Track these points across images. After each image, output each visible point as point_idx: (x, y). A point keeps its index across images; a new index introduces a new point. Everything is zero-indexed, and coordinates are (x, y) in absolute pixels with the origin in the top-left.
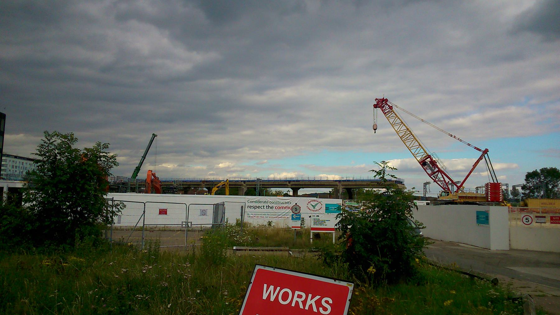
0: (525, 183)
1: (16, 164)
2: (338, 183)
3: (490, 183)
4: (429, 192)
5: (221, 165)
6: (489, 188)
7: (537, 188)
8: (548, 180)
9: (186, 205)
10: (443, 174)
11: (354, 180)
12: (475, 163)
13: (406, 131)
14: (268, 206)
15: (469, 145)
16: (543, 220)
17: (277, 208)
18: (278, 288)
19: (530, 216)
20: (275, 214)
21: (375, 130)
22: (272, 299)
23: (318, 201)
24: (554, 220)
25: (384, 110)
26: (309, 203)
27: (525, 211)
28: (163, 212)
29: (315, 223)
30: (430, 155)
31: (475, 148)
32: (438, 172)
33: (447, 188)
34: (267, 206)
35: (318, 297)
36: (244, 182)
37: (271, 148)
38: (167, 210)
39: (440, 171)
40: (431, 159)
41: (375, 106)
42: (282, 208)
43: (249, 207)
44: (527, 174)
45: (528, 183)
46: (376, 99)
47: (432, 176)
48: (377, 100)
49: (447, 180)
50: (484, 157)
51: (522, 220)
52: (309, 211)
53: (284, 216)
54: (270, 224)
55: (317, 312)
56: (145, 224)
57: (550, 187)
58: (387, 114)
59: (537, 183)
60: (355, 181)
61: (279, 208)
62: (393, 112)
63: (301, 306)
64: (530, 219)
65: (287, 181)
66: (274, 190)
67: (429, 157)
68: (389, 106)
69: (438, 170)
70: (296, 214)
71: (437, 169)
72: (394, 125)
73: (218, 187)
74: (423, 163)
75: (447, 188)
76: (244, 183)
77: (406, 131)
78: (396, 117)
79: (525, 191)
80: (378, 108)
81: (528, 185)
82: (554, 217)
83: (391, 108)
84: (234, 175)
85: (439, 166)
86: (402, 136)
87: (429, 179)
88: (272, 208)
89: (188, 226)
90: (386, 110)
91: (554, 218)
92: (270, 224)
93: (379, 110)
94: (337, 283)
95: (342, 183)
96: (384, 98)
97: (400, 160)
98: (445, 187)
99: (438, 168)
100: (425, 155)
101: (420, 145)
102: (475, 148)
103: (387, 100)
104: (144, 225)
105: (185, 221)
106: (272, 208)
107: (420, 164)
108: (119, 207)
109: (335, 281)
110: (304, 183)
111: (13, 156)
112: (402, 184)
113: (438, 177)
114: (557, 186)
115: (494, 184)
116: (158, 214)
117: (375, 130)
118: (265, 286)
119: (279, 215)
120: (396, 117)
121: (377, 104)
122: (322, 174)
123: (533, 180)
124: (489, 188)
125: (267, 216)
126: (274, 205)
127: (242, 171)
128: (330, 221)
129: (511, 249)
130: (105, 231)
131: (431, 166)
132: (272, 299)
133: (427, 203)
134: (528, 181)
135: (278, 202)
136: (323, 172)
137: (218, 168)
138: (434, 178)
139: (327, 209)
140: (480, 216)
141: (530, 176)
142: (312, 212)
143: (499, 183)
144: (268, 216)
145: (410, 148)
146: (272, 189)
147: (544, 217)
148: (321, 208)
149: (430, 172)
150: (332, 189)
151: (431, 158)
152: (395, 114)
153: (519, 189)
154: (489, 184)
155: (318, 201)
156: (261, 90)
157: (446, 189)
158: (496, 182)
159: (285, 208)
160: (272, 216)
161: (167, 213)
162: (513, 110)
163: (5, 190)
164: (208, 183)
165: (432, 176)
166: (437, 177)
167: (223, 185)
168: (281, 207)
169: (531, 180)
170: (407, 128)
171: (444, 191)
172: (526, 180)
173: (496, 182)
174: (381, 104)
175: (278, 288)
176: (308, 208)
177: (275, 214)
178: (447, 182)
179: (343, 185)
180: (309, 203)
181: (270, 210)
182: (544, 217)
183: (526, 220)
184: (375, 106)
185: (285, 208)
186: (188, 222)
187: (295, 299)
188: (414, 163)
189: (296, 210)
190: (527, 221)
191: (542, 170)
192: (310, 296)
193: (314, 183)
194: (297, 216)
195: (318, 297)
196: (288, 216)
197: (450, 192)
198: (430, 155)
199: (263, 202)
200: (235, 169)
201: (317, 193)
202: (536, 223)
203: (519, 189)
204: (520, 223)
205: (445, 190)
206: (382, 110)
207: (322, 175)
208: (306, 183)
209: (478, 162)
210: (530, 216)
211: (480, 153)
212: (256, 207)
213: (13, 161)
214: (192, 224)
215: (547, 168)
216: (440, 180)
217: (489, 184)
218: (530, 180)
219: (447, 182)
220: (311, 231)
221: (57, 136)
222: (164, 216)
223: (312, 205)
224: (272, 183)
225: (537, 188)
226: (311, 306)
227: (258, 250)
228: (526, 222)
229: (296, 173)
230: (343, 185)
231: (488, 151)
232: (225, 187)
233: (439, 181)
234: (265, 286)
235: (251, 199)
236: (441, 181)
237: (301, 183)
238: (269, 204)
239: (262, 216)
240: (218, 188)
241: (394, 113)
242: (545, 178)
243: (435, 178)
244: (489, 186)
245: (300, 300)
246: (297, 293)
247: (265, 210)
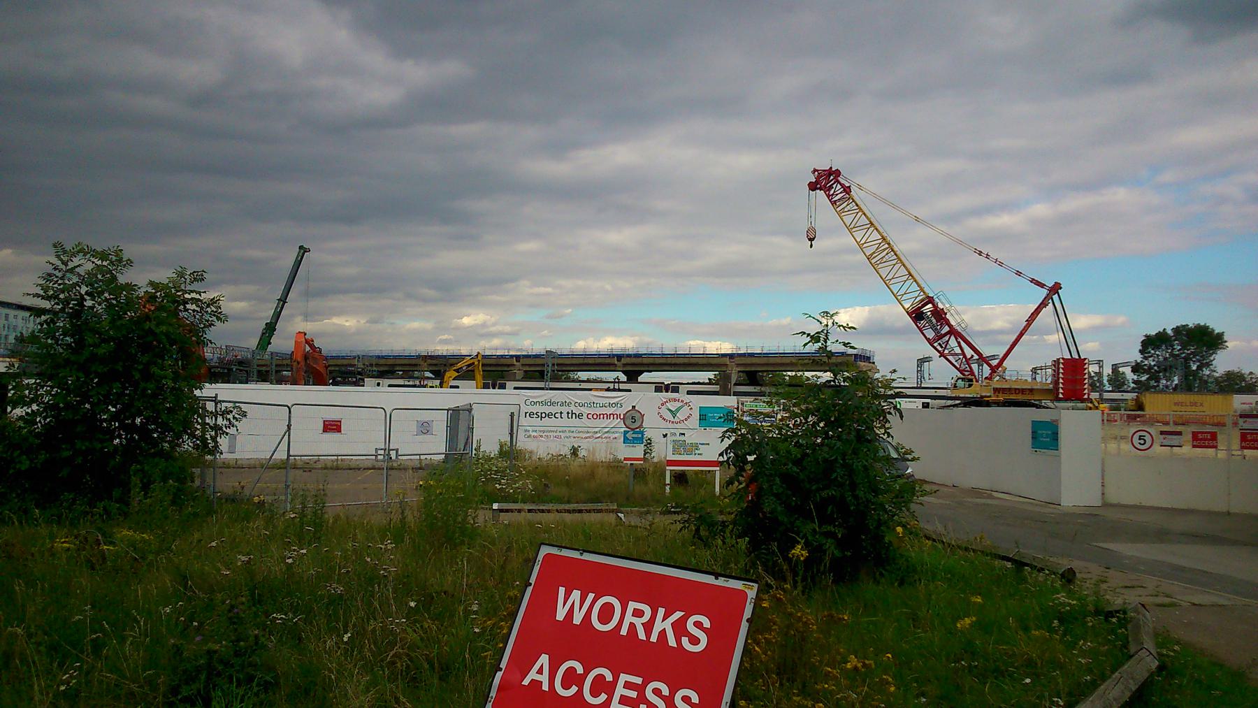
0: (1139, 358)
2: (727, 360)
3: (1063, 359)
4: (929, 379)
5: (466, 321)
6: (1061, 371)
7: (1166, 369)
8: (1189, 352)
9: (385, 411)
10: (960, 340)
11: (764, 354)
12: (1032, 314)
13: (880, 244)
14: (570, 412)
15: (1019, 273)
16: (1175, 440)
17: (590, 416)
18: (591, 596)
20: (586, 429)
21: (811, 240)
22: (578, 619)
23: (682, 401)
24: (1248, 441)
25: (833, 195)
26: (662, 404)
28: (332, 427)
29: (675, 452)
30: (933, 297)
31: (1033, 281)
32: (949, 335)
33: (968, 371)
34: (568, 413)
35: (678, 615)
36: (518, 358)
37: (580, 282)
38: (340, 421)
39: (953, 332)
40: (935, 306)
41: (813, 187)
42: (602, 416)
43: (528, 414)
44: (1144, 338)
45: (1146, 358)
46: (815, 170)
47: (936, 345)
48: (816, 173)
49: (969, 352)
50: (1050, 301)
53: (606, 435)
54: (575, 452)
55: (676, 646)
56: (291, 453)
57: (1194, 368)
58: (838, 204)
59: (1165, 359)
60: (766, 355)
61: (595, 417)
62: (852, 199)
63: (642, 635)
64: (1148, 438)
65: (614, 356)
66: (583, 375)
67: (930, 300)
68: (842, 185)
69: (948, 329)
70: (633, 429)
71: (946, 329)
72: (854, 230)
73: (457, 371)
74: (917, 315)
75: (968, 371)
76: (516, 361)
77: (880, 244)
78: (858, 211)
79: (1138, 376)
80: (818, 191)
81: (1146, 362)
82: (1200, 432)
83: (847, 190)
84: (496, 342)
85: (953, 323)
86: (871, 255)
87: (929, 351)
88: (580, 416)
89: (391, 458)
90: (837, 195)
91: (1199, 435)
92: (575, 452)
93: (820, 193)
94: (721, 582)
95: (737, 360)
96: (831, 168)
97: (867, 308)
98: (963, 367)
99: (949, 326)
100: (921, 297)
101: (910, 274)
102: (1033, 281)
103: (838, 173)
104: (289, 455)
105: (383, 447)
106: (580, 416)
107: (911, 317)
108: (230, 416)
109: (717, 578)
110: (651, 361)
112: (870, 363)
113: (948, 347)
114: (1208, 365)
115: (1072, 359)
116: (321, 431)
117: (811, 240)
118: (562, 590)
119: (597, 432)
120: (858, 211)
121: (817, 182)
122: (692, 340)
123: (1157, 353)
124: (1061, 371)
125: (568, 434)
126: (585, 411)
127: (515, 334)
128: (708, 444)
129: (1106, 505)
131: (934, 321)
132: (578, 619)
133: (923, 403)
134: (1146, 355)
135: (594, 403)
136: (697, 336)
137: (458, 328)
138: (940, 349)
139: (703, 418)
141: (1150, 343)
142: (671, 426)
143: (1082, 358)
144: (571, 434)
145: (887, 282)
146: (579, 373)
148: (689, 417)
149: (931, 334)
150: (714, 373)
151: (933, 305)
152: (857, 205)
153: (1127, 371)
154: (1061, 361)
155: (682, 401)
156: (558, 149)
157: (967, 373)
158: (1077, 357)
159: (608, 416)
160: (581, 435)
161: (342, 429)
162: (1120, 195)
164: (434, 362)
165: (936, 345)
166: (946, 346)
167: (469, 366)
168: (600, 415)
169: (1153, 352)
170: (882, 237)
171: (962, 376)
172: (1141, 352)
173: (1077, 357)
174: (825, 180)
175: (591, 596)
176: (661, 416)
177: (586, 429)
178: (969, 357)
179: (738, 365)
180: (662, 404)
181: (575, 421)
182: (1179, 433)
183: (1140, 439)
184: (813, 187)
185: (608, 416)
186: (389, 450)
187: (629, 618)
188: (897, 314)
189: (633, 420)
190: (1142, 442)
191: (1177, 330)
192: (661, 611)
193: (674, 361)
194: (634, 436)
195: (678, 615)
196: (616, 435)
197: (974, 380)
198: (933, 297)
199: (559, 404)
200: (499, 328)
202: (1161, 446)
203: (1127, 371)
204: (1126, 447)
205: (964, 375)
206: (828, 196)
207: (692, 343)
208: (658, 361)
209: (1037, 311)
211: (1044, 292)
212: (544, 415)
214: (399, 453)
215: (1187, 325)
216: (953, 352)
217: (1061, 361)
218: (1150, 352)
219: (969, 357)
220: (668, 468)
221: (1222, 363)
222: (335, 436)
224: (581, 361)
225: (1166, 369)
226: (663, 633)
227: (549, 511)
228: (1140, 443)
229: (637, 338)
230: (738, 365)
231: (1061, 288)
232: (473, 371)
233: (952, 355)
234: (562, 590)
235: (535, 397)
236: (956, 354)
237: (645, 361)
238: (572, 408)
239: (558, 434)
240: (458, 372)
241: (854, 201)
242: (1184, 347)
243: (942, 347)
244: (1061, 366)
245: (639, 622)
246: (632, 605)
247: (565, 421)
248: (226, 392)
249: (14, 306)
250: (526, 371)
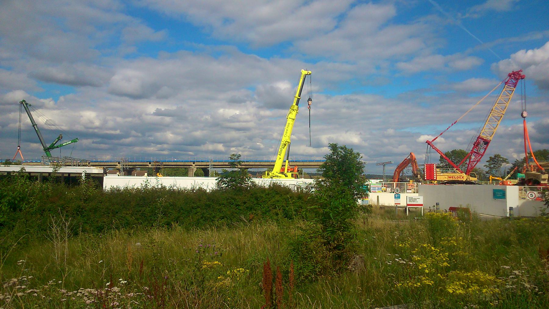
19: (530, 198)
27: (502, 158)
51: (528, 196)
70: (397, 194)
130: (390, 188)
134: (442, 162)
140: (497, 193)
163: (83, 175)
183: (531, 195)
190: (532, 196)
194: (398, 196)
201: (314, 173)
210: (530, 198)
220: (407, 206)
250: (197, 168)
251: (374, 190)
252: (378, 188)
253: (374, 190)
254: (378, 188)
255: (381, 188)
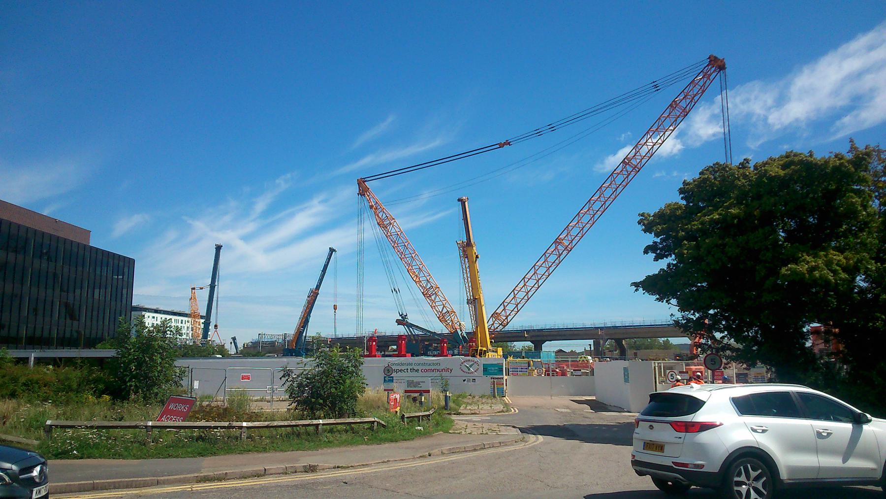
1: (157, 321)
17: (423, 371)
26: (462, 363)
34: (411, 369)
52: (462, 374)
61: (425, 371)
64: (670, 377)
88: (417, 371)
106: (417, 371)
111: (153, 309)
126: (420, 368)
142: (467, 375)
147: (506, 380)
159: (433, 371)
176: (462, 370)
185: (433, 371)
190: (672, 377)
212: (398, 371)
213: (154, 317)
223: (466, 366)
248: (180, 363)
249: (153, 311)
251: (516, 371)
252: (522, 369)
253: (516, 371)
254: (522, 369)
255: (526, 369)
